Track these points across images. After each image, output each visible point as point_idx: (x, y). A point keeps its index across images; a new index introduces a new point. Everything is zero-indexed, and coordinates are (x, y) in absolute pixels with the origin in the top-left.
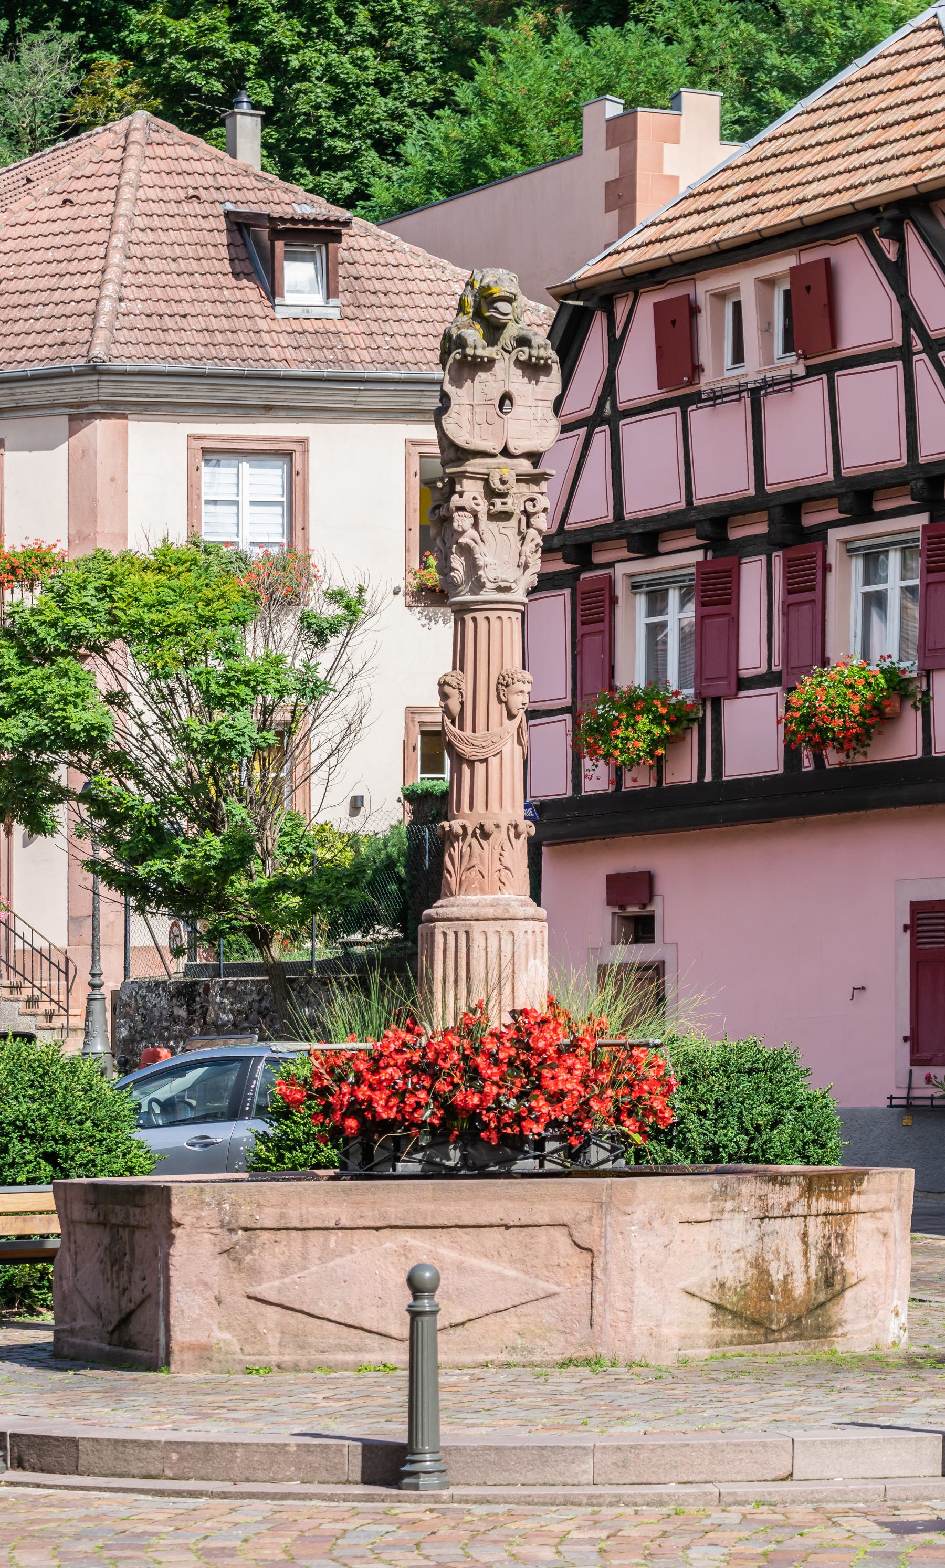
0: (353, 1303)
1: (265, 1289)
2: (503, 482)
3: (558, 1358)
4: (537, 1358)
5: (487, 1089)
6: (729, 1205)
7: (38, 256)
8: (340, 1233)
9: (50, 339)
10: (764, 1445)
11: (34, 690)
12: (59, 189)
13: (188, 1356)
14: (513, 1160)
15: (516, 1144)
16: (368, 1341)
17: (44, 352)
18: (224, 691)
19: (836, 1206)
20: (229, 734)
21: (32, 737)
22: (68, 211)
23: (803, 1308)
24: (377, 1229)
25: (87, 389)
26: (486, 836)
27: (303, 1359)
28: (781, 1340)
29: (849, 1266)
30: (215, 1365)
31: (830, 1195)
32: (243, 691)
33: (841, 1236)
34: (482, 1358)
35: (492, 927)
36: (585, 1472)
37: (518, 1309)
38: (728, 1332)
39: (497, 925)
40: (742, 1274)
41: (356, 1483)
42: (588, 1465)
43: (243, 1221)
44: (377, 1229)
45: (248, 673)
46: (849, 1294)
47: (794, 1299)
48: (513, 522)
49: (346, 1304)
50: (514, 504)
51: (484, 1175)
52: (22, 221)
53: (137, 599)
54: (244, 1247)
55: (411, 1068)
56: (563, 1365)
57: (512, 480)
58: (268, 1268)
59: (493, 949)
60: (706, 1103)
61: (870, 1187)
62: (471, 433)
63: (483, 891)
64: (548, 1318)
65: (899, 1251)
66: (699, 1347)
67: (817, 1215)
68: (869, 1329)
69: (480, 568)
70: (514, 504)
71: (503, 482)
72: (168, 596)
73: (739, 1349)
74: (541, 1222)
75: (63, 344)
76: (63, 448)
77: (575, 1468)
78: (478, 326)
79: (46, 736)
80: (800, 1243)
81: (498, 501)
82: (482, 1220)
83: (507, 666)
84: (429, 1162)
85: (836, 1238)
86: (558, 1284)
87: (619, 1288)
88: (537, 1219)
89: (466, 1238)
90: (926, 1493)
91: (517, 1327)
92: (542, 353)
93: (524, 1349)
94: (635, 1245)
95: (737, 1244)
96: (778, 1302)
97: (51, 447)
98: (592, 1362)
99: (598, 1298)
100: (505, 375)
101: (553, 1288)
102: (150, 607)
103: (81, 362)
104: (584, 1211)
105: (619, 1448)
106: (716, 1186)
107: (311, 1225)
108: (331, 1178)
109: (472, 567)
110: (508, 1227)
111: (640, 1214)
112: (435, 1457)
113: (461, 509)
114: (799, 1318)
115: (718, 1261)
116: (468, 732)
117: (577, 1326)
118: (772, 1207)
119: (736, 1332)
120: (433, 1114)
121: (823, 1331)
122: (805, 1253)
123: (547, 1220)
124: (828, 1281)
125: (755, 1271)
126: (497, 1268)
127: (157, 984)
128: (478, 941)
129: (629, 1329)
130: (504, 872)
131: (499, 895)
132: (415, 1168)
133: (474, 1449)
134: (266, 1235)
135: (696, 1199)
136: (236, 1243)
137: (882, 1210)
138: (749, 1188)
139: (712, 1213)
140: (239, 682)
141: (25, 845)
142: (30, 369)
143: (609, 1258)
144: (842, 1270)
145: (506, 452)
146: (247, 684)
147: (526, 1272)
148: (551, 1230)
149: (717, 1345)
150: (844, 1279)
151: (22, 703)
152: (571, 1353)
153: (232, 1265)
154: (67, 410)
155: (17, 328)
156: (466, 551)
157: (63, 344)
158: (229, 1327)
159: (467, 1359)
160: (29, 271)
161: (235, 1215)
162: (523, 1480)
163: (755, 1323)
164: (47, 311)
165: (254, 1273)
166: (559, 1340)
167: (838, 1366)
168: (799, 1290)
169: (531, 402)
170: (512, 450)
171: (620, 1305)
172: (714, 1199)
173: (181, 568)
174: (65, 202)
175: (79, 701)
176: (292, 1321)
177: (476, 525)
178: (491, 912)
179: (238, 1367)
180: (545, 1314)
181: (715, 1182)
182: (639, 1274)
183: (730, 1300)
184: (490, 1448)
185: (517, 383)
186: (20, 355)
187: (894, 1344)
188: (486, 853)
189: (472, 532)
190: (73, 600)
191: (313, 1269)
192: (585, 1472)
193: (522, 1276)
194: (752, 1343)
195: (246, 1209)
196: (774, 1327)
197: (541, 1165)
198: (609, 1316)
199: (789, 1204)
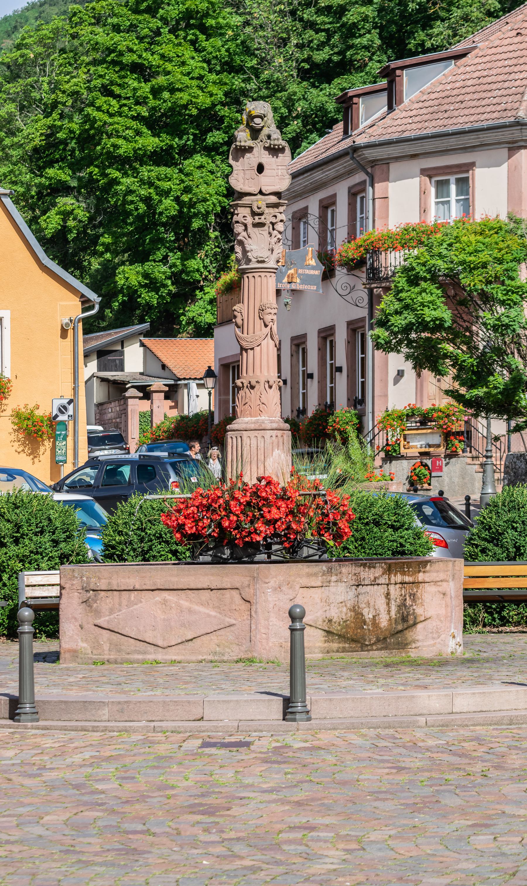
0: (141, 629)
1: (101, 622)
2: (259, 208)
3: (235, 658)
4: (225, 658)
5: (231, 518)
6: (334, 578)
7: (500, 64)
8: (136, 592)
9: (499, 108)
10: (189, 702)
11: (412, 300)
12: (516, 27)
13: (67, 655)
14: (255, 555)
15: (255, 547)
16: (149, 649)
17: (496, 115)
18: (505, 298)
19: (407, 579)
20: (506, 320)
21: (407, 325)
22: (519, 39)
23: (387, 633)
24: (153, 590)
25: (515, 134)
26: (253, 387)
27: (119, 658)
28: (372, 650)
29: (419, 611)
30: (79, 660)
31: (403, 573)
32: (515, 297)
33: (413, 596)
34: (200, 658)
35: (252, 434)
36: (104, 715)
37: (217, 633)
38: (335, 646)
39: (256, 433)
40: (343, 615)
41: (6, 719)
42: (106, 711)
43: (92, 586)
44: (153, 590)
45: (519, 287)
46: (419, 626)
47: (381, 628)
48: (266, 228)
49: (138, 629)
50: (267, 218)
51: (241, 562)
52: (495, 45)
53: (464, 250)
54: (93, 600)
55: (200, 506)
56: (237, 662)
57: (264, 207)
58: (104, 610)
59: (254, 445)
60: (516, 523)
61: (432, 568)
62: (244, 184)
63: (251, 416)
64: (231, 637)
65: (453, 603)
66: (314, 653)
67: (396, 584)
68: (434, 645)
69: (248, 252)
70: (262, 220)
71: (259, 208)
72: (481, 247)
73: (342, 654)
74: (226, 587)
75: (505, 110)
76: (505, 165)
77: (100, 712)
78: (248, 130)
79: (413, 324)
80: (384, 598)
81: (257, 218)
82: (199, 586)
83: (265, 301)
84: (214, 556)
85: (410, 596)
86: (235, 619)
87: (262, 622)
88: (224, 586)
89: (193, 595)
90: (260, 728)
91: (216, 641)
92: (276, 142)
93: (220, 653)
94: (270, 599)
95: (341, 599)
96: (369, 630)
97: (499, 165)
98: (251, 661)
99: (253, 627)
100: (259, 155)
101: (234, 622)
102: (471, 254)
103: (512, 119)
104: (246, 581)
105: (119, 703)
106: (324, 568)
107: (122, 588)
108: (174, 564)
109: (245, 252)
110: (212, 590)
111: (273, 583)
112: (32, 705)
113: (237, 222)
114: (385, 639)
115: (328, 608)
116: (245, 335)
117: (244, 641)
118: (364, 579)
119: (341, 645)
120: (214, 531)
121: (403, 646)
122: (388, 604)
123: (229, 586)
124: (404, 619)
125: (353, 614)
126: (207, 611)
127: (521, 455)
128: (246, 441)
129: (268, 643)
130: (262, 406)
131: (259, 418)
132: (208, 559)
133: (55, 702)
134: (103, 593)
135: (309, 575)
136: (89, 598)
137: (442, 581)
138: (347, 569)
139: (322, 582)
140: (513, 293)
141: (395, 384)
142: (485, 124)
143: (258, 605)
144: (414, 613)
145: (261, 192)
146: (517, 293)
147: (220, 613)
148: (232, 591)
149: (328, 652)
150: (415, 618)
151: (407, 307)
152: (242, 656)
153: (88, 608)
154: (507, 145)
155: (484, 103)
156: (241, 243)
157: (505, 110)
158: (86, 640)
159: (194, 658)
160: (494, 72)
161: (88, 583)
162: (76, 718)
163: (353, 641)
164: (500, 93)
165: (98, 613)
166: (235, 648)
167: (414, 664)
168: (384, 622)
169: (275, 167)
170: (264, 191)
171: (263, 631)
172: (323, 575)
173: (492, 232)
174: (518, 34)
175: (430, 305)
176: (115, 638)
177: (246, 229)
178: (252, 426)
179: (90, 661)
180: (229, 635)
181: (324, 567)
182: (272, 614)
183: (336, 628)
184: (62, 702)
185: (266, 158)
186: (483, 117)
187: (452, 653)
188: (253, 396)
189: (244, 234)
190: (436, 251)
191: (124, 611)
192: (104, 715)
193: (218, 615)
194: (352, 651)
195: (93, 580)
196: (367, 643)
197: (269, 557)
198: (258, 637)
199: (375, 578)
